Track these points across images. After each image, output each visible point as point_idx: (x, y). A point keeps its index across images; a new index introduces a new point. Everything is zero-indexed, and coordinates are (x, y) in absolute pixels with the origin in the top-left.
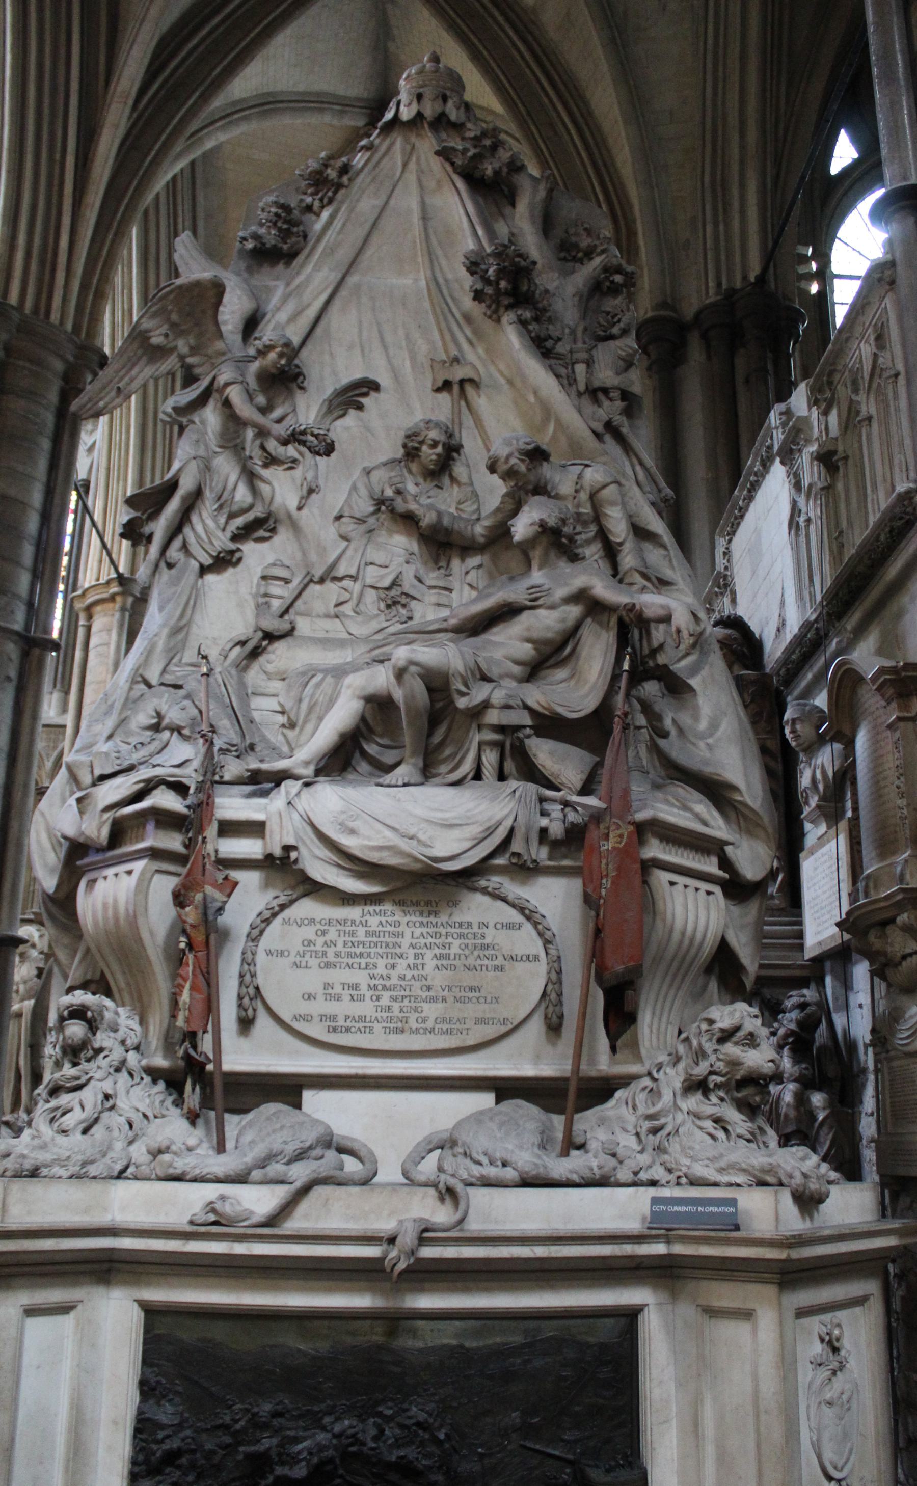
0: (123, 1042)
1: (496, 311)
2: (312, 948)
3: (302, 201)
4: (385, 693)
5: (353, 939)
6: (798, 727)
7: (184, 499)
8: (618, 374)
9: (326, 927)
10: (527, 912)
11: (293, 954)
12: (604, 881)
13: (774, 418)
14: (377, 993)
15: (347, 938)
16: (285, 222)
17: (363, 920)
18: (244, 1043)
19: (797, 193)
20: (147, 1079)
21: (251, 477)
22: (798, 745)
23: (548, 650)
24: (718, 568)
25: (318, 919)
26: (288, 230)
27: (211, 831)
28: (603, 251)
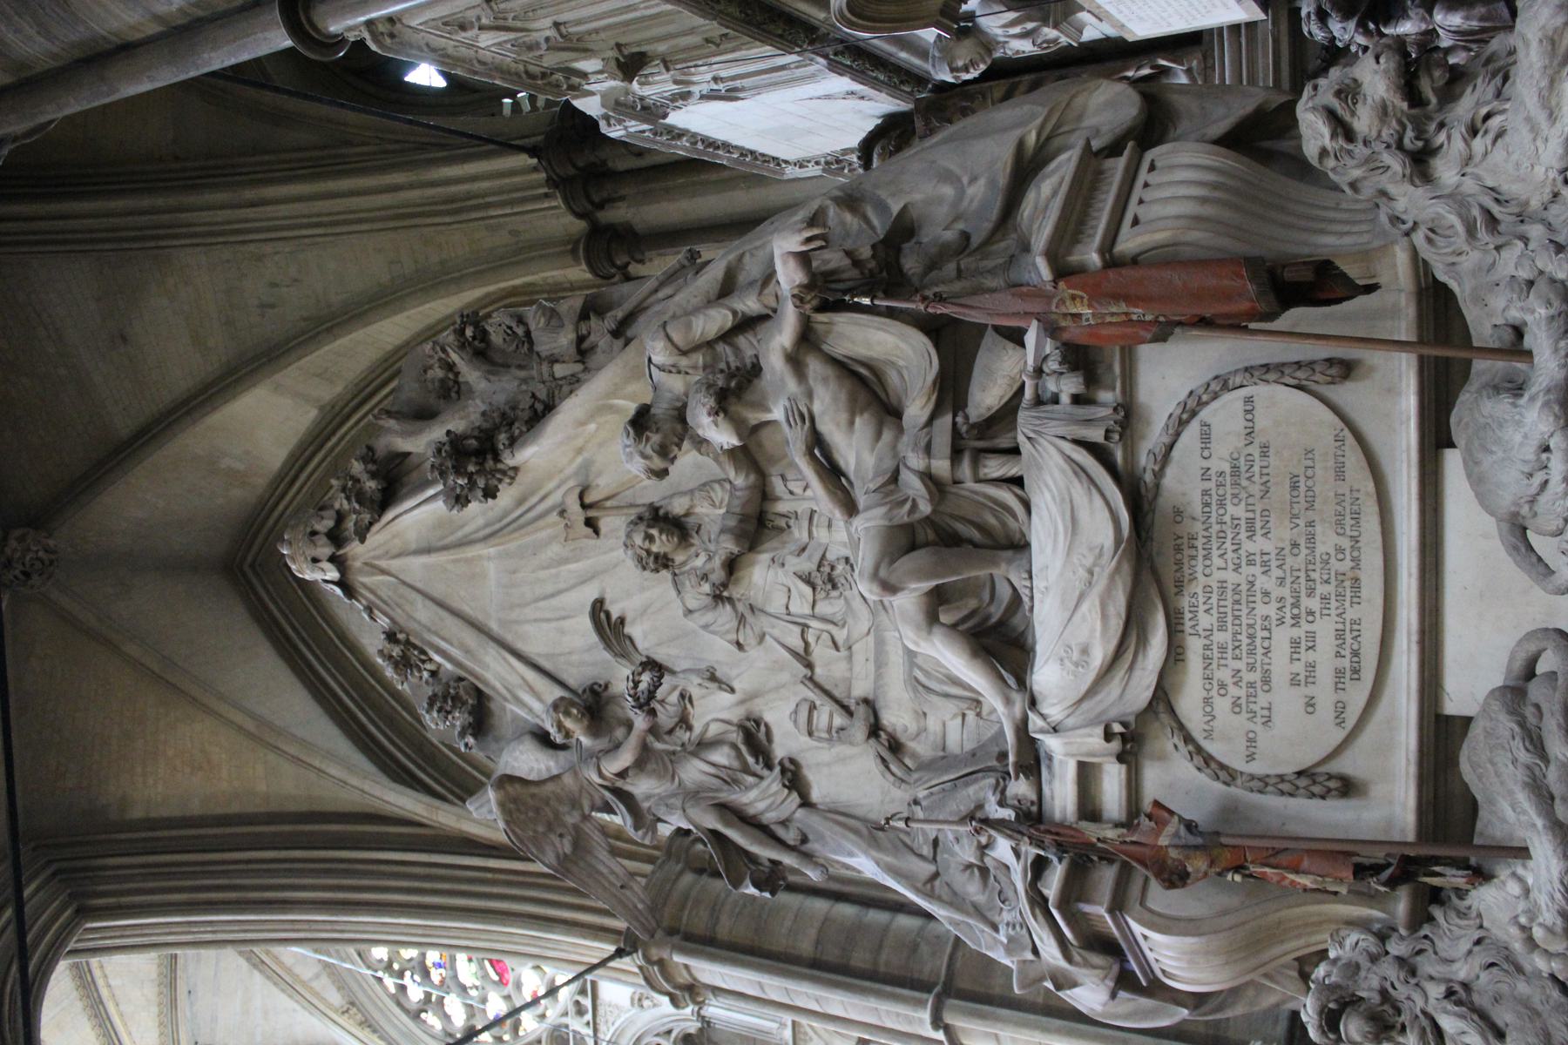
0: (1374, 959)
1: (504, 473)
2: (1243, 701)
4: (924, 599)
5: (1230, 647)
6: (960, 63)
7: (728, 824)
8: (562, 326)
9: (1215, 683)
11: (1252, 726)
12: (1135, 317)
13: (615, 132)
14: (1303, 615)
15: (1229, 655)
16: (445, 701)
18: (1377, 791)
21: (703, 746)
23: (863, 396)
24: (819, 173)
25: (1205, 694)
26: (453, 699)
27: (1092, 831)
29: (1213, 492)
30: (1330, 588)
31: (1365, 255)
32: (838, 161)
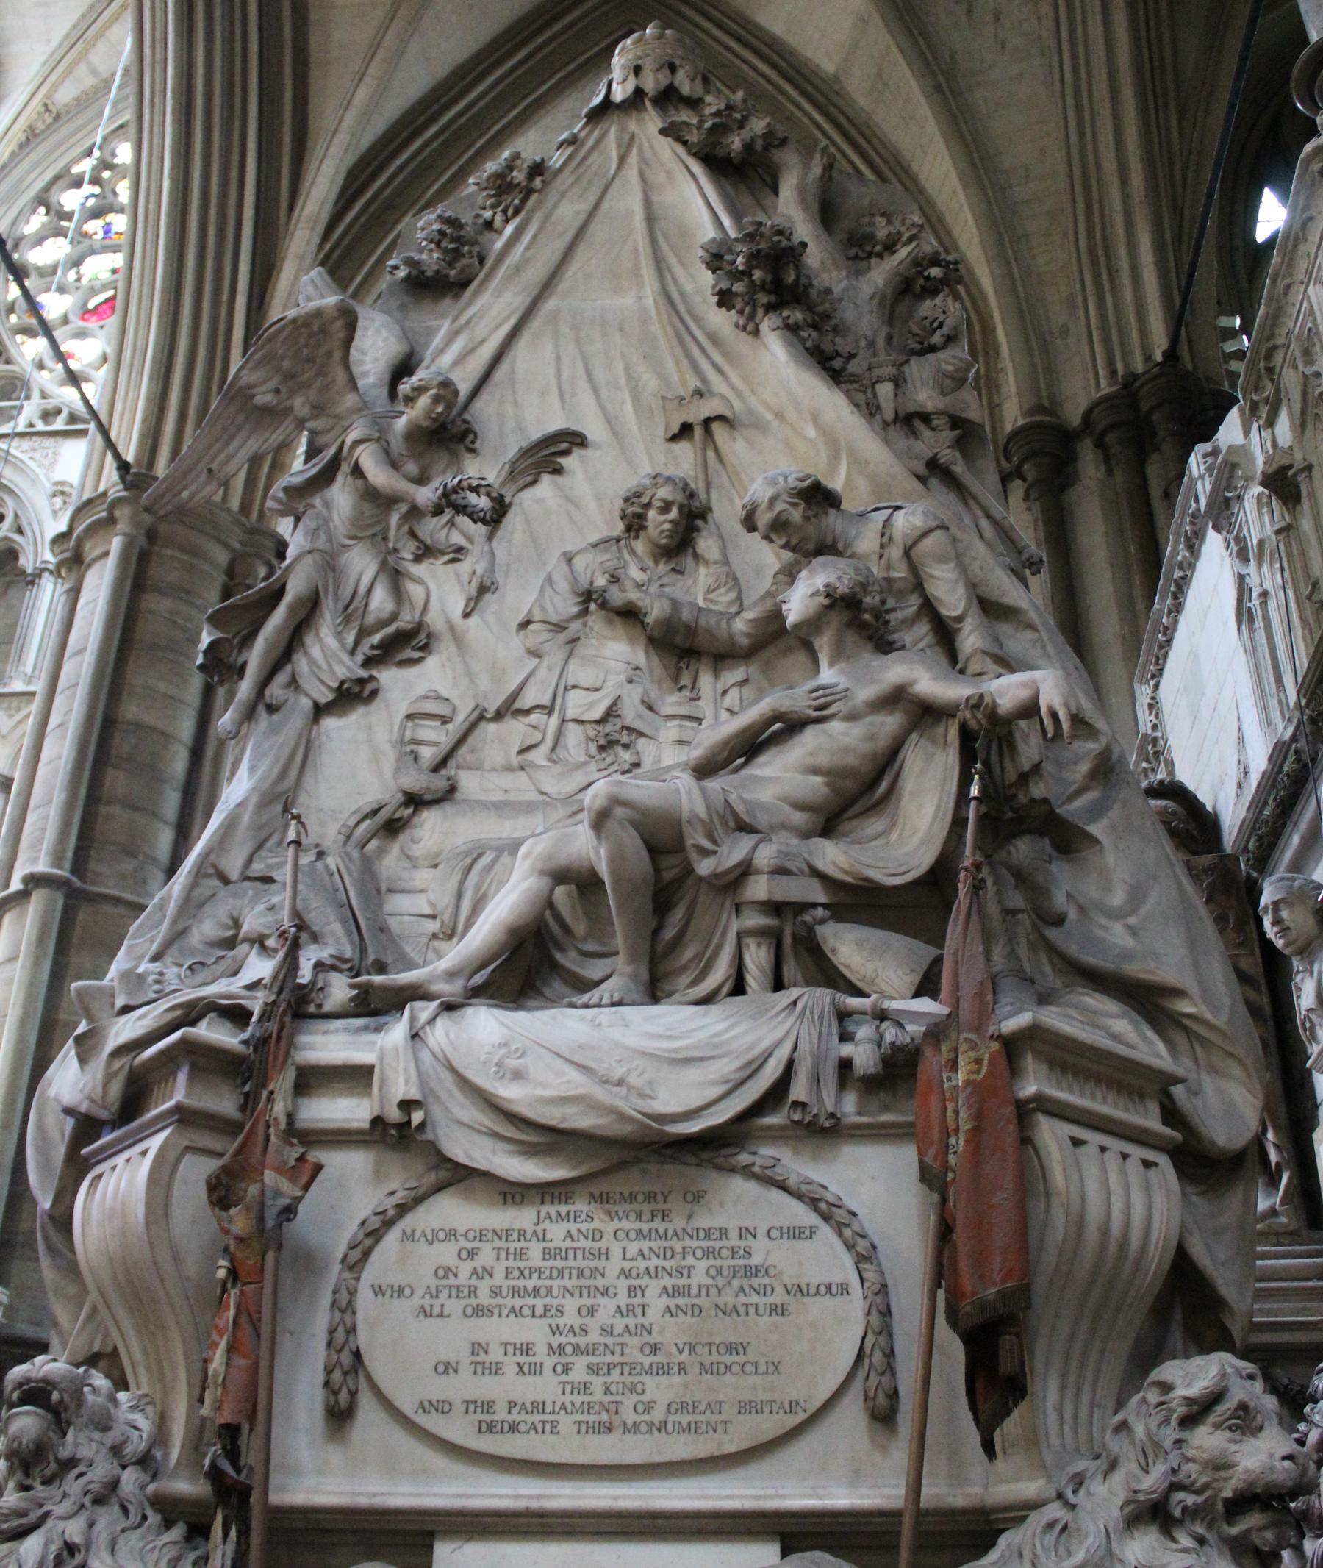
0: (116, 1450)
1: (751, 317)
2: (452, 1281)
3: (478, 216)
4: (586, 864)
5: (522, 1264)
6: (1285, 914)
7: (292, 609)
9: (476, 1244)
10: (823, 1206)
11: (420, 1292)
12: (952, 1141)
13: (1196, 463)
14: (564, 1360)
15: (511, 1263)
16: (453, 240)
17: (539, 1230)
18: (335, 1455)
19: (1205, 217)
20: (154, 1518)
21: (395, 577)
22: (1286, 946)
23: (850, 786)
24: (1142, 729)
25: (461, 1231)
26: (456, 250)
27: (283, 1083)
28: (911, 239)
29: (724, 1243)
30: (598, 1395)
31: (1033, 1441)
32: (1157, 754)
